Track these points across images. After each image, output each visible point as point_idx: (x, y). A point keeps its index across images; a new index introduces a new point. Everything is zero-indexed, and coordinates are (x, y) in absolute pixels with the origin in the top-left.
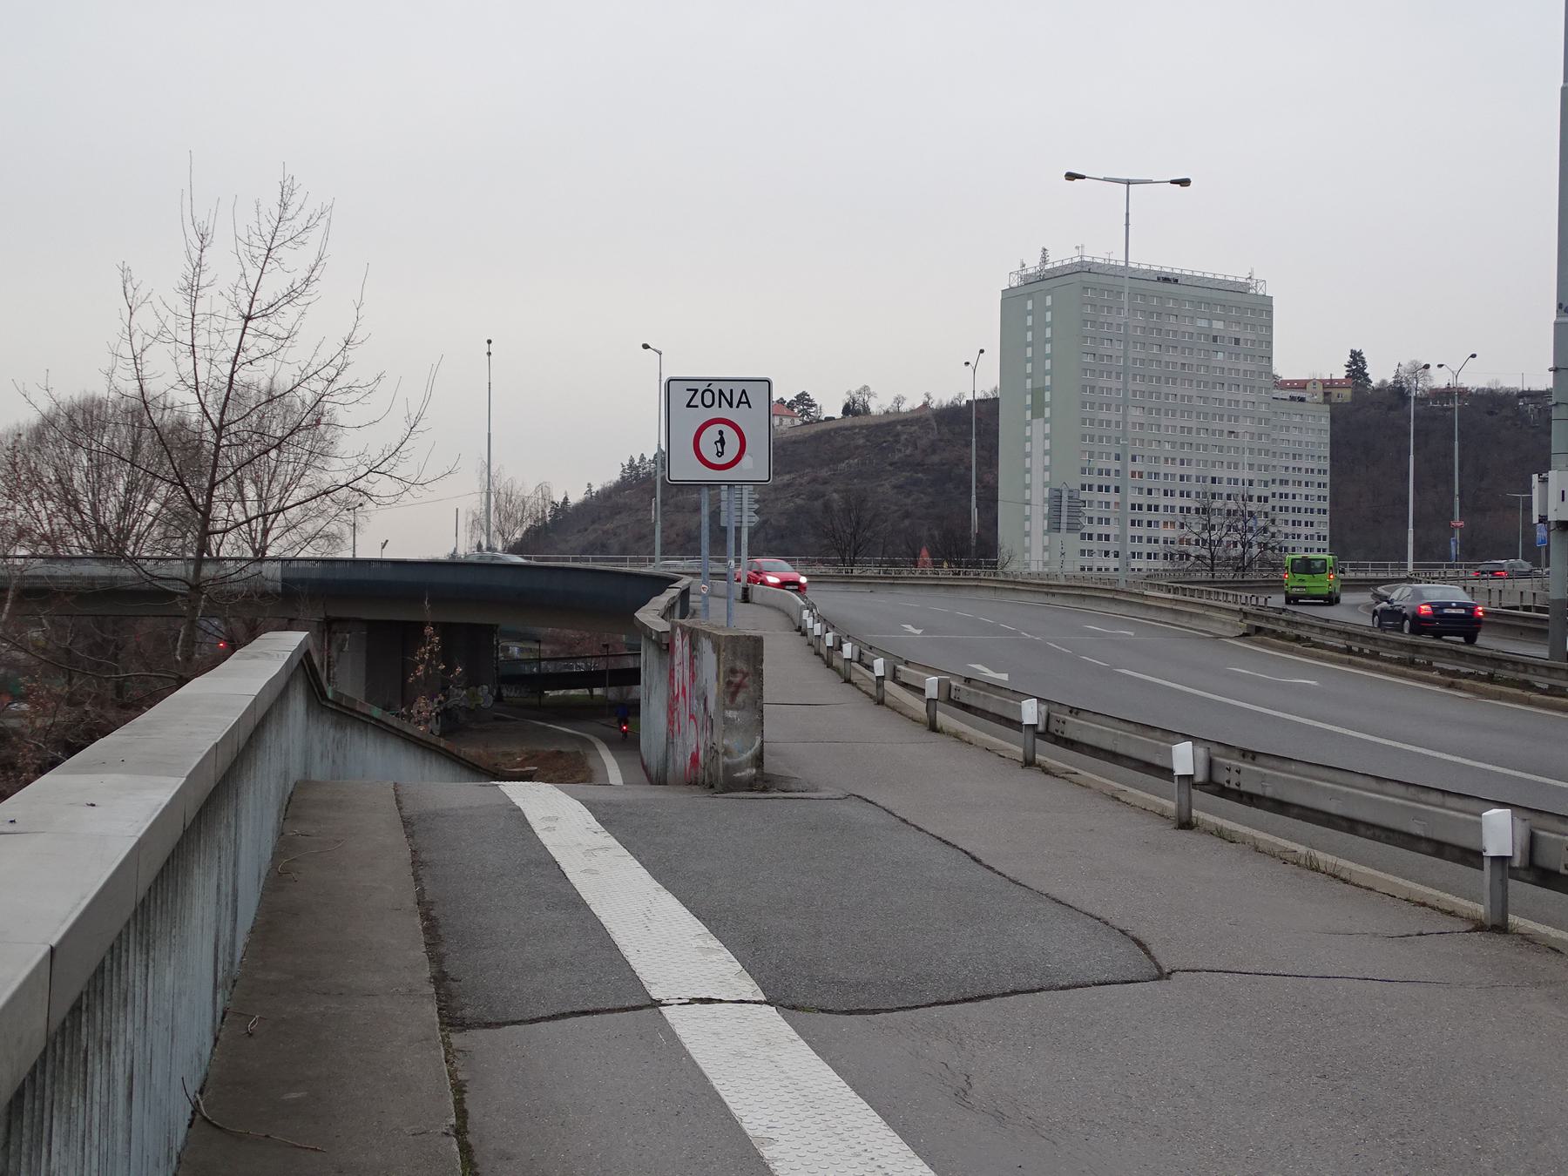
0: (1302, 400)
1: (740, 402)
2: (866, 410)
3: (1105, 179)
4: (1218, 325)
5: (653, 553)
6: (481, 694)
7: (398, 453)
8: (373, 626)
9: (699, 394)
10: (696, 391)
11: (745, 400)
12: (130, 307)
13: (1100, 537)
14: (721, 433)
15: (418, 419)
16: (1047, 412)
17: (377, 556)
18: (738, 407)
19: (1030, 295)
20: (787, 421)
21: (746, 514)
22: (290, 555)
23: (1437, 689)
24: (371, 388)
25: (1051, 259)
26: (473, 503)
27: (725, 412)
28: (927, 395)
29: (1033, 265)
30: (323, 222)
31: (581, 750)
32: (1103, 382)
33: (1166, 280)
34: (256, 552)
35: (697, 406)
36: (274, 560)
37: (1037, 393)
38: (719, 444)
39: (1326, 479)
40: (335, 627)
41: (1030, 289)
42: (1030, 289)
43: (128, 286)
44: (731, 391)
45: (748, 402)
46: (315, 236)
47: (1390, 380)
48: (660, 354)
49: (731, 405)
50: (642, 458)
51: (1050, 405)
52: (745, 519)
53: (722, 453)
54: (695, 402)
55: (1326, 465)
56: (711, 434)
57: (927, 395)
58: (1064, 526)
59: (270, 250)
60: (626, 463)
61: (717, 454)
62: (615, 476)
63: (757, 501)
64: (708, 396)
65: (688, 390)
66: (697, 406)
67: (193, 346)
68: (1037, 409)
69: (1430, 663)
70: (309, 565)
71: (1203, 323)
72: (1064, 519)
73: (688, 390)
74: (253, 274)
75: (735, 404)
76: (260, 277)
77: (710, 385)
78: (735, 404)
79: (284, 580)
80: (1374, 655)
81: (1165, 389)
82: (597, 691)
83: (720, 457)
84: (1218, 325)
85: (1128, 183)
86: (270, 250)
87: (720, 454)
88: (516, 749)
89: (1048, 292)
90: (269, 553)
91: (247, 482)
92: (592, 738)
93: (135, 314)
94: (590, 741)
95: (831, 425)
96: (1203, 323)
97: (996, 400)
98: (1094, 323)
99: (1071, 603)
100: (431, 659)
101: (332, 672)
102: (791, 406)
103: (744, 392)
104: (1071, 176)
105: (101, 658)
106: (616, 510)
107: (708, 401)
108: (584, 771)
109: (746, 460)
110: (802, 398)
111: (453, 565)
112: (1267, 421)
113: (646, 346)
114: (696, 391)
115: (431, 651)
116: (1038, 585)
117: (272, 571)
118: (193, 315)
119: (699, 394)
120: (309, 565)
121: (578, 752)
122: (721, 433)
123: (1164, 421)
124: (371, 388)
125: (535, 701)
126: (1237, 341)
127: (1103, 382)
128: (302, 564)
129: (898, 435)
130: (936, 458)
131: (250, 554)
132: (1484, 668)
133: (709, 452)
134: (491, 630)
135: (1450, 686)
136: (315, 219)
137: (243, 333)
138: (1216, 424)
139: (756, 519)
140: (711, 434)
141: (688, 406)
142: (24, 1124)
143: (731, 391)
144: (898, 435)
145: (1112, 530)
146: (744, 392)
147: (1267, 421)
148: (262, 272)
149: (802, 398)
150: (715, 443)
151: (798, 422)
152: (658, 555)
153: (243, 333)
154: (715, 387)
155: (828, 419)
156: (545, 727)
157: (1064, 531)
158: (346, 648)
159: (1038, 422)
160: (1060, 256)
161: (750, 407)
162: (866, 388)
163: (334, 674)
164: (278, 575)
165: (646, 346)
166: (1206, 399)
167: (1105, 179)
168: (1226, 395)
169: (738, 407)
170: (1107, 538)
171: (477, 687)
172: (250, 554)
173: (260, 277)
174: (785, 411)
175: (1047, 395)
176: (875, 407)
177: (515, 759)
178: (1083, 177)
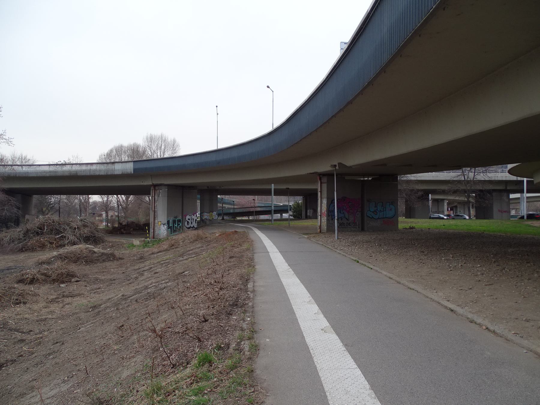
6: (214, 215)
8: (169, 186)
31: (246, 231)
40: (157, 188)
48: (273, 92)
88: (216, 231)
94: (250, 228)
101: (155, 204)
108: (249, 242)
113: (268, 87)
121: (245, 231)
142: (400, 210)
156: (234, 225)
158: (160, 196)
163: (156, 205)
165: (268, 87)
171: (212, 212)
177: (215, 235)
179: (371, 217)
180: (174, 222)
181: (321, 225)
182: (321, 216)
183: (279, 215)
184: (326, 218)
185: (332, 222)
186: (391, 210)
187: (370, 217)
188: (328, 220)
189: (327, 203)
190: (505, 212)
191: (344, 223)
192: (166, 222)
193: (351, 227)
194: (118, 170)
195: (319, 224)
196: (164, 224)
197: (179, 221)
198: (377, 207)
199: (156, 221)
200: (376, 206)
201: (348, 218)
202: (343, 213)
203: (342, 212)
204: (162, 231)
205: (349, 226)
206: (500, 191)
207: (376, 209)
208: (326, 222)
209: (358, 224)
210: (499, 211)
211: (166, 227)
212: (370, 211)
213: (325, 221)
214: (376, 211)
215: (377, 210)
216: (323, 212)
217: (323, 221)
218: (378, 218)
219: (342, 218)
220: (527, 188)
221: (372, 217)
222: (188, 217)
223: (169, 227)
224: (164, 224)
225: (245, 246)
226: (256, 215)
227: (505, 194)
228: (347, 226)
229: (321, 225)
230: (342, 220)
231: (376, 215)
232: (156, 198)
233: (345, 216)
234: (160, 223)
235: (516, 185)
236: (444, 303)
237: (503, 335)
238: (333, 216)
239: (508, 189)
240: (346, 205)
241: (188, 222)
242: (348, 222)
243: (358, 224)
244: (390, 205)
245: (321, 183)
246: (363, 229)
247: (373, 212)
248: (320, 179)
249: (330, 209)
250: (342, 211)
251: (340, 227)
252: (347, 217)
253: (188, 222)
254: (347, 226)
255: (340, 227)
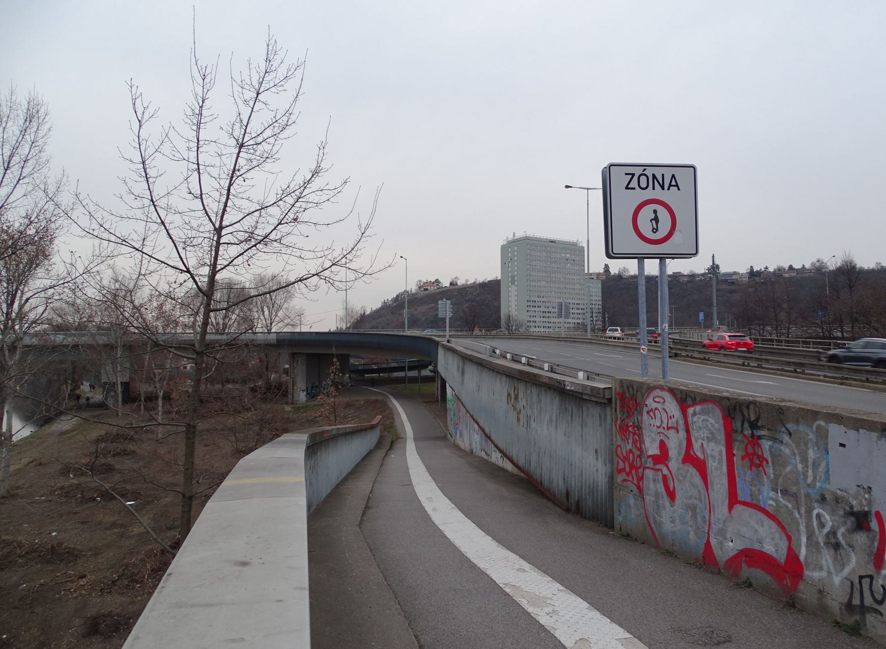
0: (592, 279)
1: (670, 185)
2: (457, 284)
3: (580, 188)
4: (568, 255)
5: (404, 328)
7: (354, 252)
8: (308, 355)
9: (636, 178)
10: (633, 175)
11: (674, 183)
12: (140, 121)
13: (533, 322)
14: (655, 212)
15: (368, 226)
16: (516, 283)
17: (308, 331)
18: (669, 189)
19: (510, 247)
20: (432, 288)
21: (448, 313)
22: (279, 331)
23: (836, 385)
24: (339, 189)
25: (516, 236)
26: (341, 313)
27: (657, 193)
28: (476, 279)
29: (511, 237)
30: (299, 73)
32: (533, 273)
33: (552, 242)
34: (268, 330)
35: (634, 189)
36: (274, 333)
37: (513, 277)
38: (654, 222)
39: (601, 303)
40: (295, 356)
41: (510, 245)
42: (510, 245)
43: (138, 102)
44: (663, 175)
45: (677, 185)
46: (291, 86)
47: (617, 273)
49: (663, 187)
50: (388, 300)
51: (516, 281)
52: (447, 315)
53: (657, 230)
54: (634, 184)
55: (600, 299)
56: (646, 213)
57: (476, 279)
58: (563, 316)
59: (258, 94)
60: (383, 301)
61: (653, 231)
62: (380, 306)
63: (452, 308)
64: (643, 180)
65: (626, 174)
66: (634, 189)
67: (198, 164)
68: (513, 283)
69: (803, 371)
70: (286, 334)
71: (564, 255)
72: (563, 313)
73: (626, 174)
74: (245, 112)
75: (666, 186)
76: (251, 115)
77: (644, 170)
78: (666, 186)
79: (277, 340)
80: (760, 366)
81: (552, 275)
82: (382, 375)
83: (655, 233)
84: (568, 255)
85: (588, 189)
86: (258, 94)
87: (655, 230)
89: (515, 246)
90: (272, 331)
91: (265, 307)
92: (387, 394)
93: (143, 127)
95: (446, 288)
96: (564, 255)
97: (500, 280)
98: (530, 255)
99: (556, 342)
100: (336, 372)
102: (433, 283)
103: (673, 176)
104: (567, 187)
105: (207, 374)
106: (380, 317)
107: (643, 184)
109: (676, 235)
110: (437, 281)
111: (338, 334)
112: (584, 285)
113: (401, 257)
114: (633, 175)
115: (336, 368)
116: (553, 337)
117: (273, 337)
118: (198, 141)
119: (636, 178)
120: (286, 334)
122: (655, 212)
123: (552, 286)
124: (339, 189)
125: (362, 378)
126: (574, 260)
127: (533, 273)
128: (283, 334)
129: (467, 291)
130: (478, 299)
131: (266, 331)
132: (864, 375)
133: (646, 228)
134: (348, 356)
135: (842, 384)
136: (293, 70)
137: (238, 156)
138: (568, 286)
139: (451, 315)
140: (646, 213)
141: (627, 188)
143: (663, 175)
144: (467, 291)
145: (537, 319)
146: (673, 176)
147: (584, 285)
148: (252, 111)
149: (437, 281)
150: (651, 221)
151: (436, 288)
152: (406, 329)
153: (238, 156)
154: (649, 172)
155: (445, 287)
157: (563, 317)
158: (299, 363)
159: (513, 286)
160: (520, 234)
161: (679, 189)
162: (457, 277)
164: (275, 338)
165: (401, 257)
166: (565, 279)
167: (580, 188)
168: (571, 277)
169: (669, 189)
170: (535, 322)
172: (266, 331)
173: (251, 115)
174: (432, 285)
175: (516, 278)
176: (460, 283)
178: (571, 187)
180: (312, 388)
192: (305, 388)
194: (261, 340)
196: (303, 391)
197: (317, 387)
199: (295, 388)
204: (302, 397)
211: (305, 393)
222: (324, 383)
223: (308, 394)
224: (303, 391)
225: (388, 412)
226: (389, 372)
232: (295, 365)
234: (299, 389)
236: (661, 488)
241: (324, 388)
253: (324, 388)
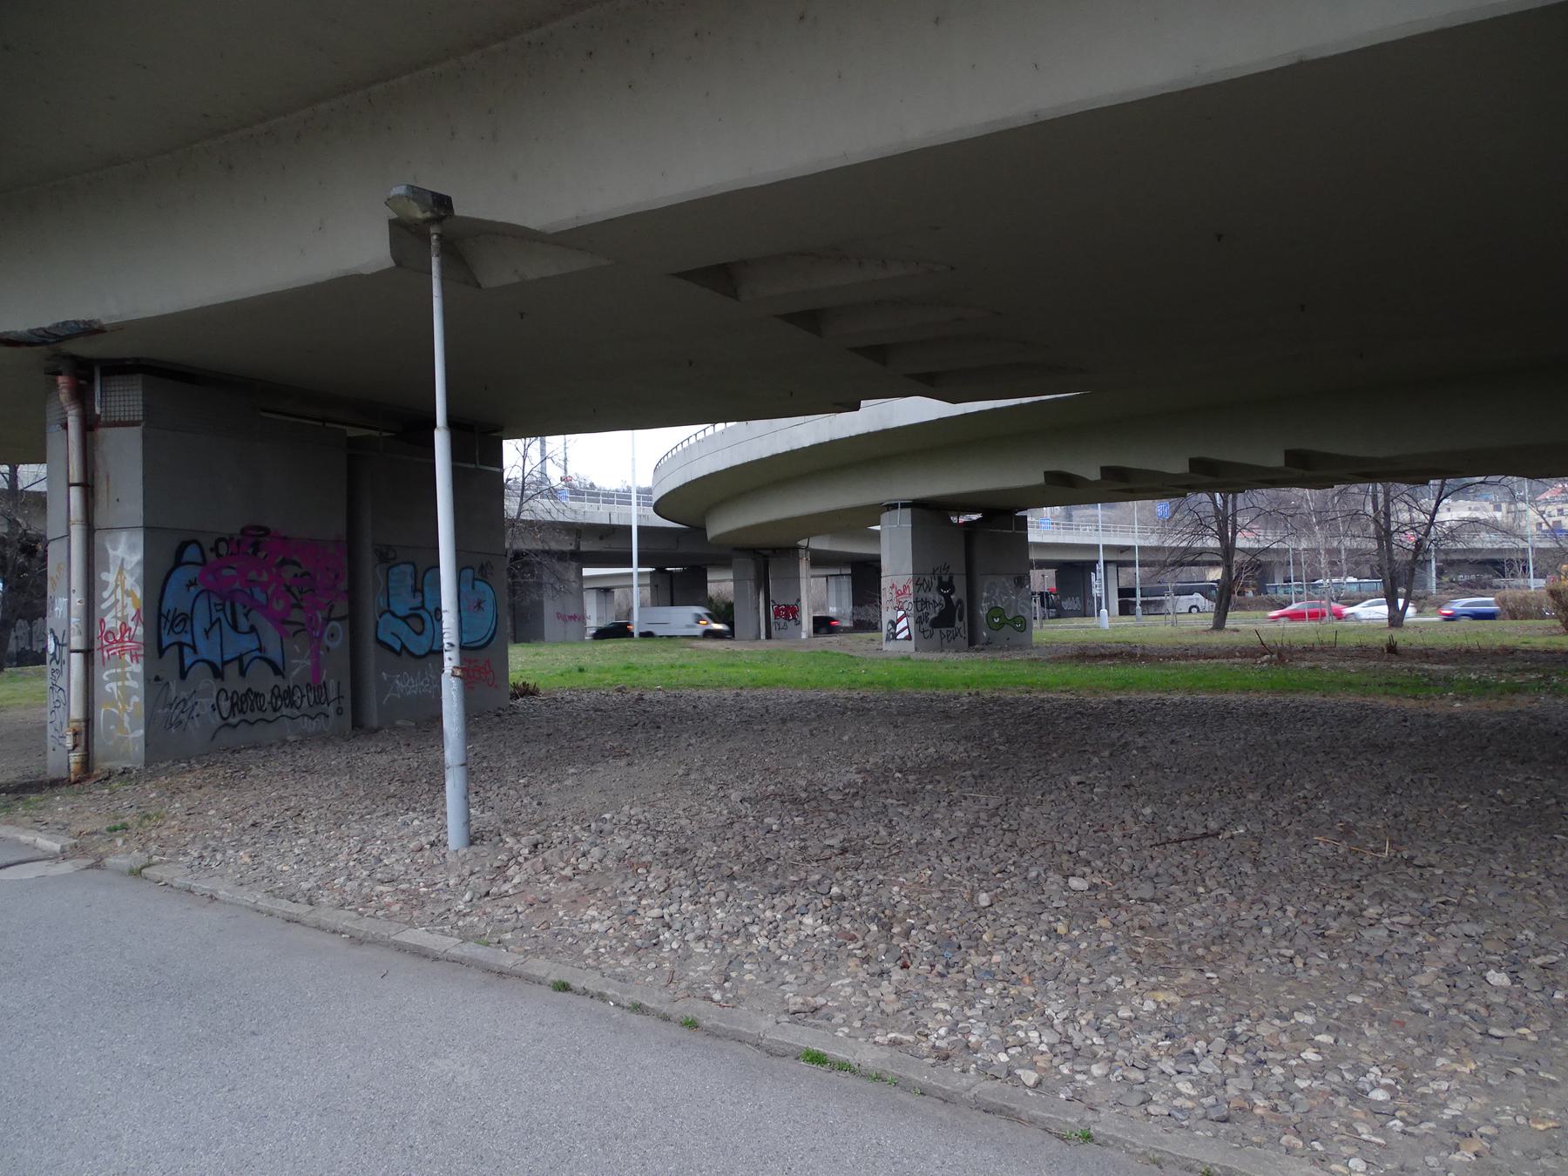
179: (397, 647)
181: (89, 720)
182: (88, 653)
183: (583, 548)
184: (137, 668)
185: (184, 694)
186: (479, 604)
187: (391, 649)
188: (153, 681)
189: (147, 563)
190: (573, 617)
191: (257, 695)
193: (297, 713)
195: (76, 712)
198: (422, 592)
200: (419, 586)
201: (279, 662)
202: (253, 629)
203: (244, 624)
205: (285, 711)
206: (562, 556)
207: (417, 602)
208: (138, 699)
209: (333, 695)
210: (559, 616)
212: (393, 614)
213: (127, 693)
214: (419, 612)
215: (423, 607)
216: (111, 622)
217: (112, 687)
218: (427, 650)
219: (246, 660)
220: (638, 549)
221: (403, 646)
227: (574, 565)
228: (275, 710)
229: (89, 720)
230: (243, 673)
231: (419, 634)
233: (260, 649)
235: (601, 538)
237: (671, 1015)
238: (187, 650)
239: (584, 552)
240: (265, 577)
242: (283, 687)
243: (333, 695)
244: (477, 583)
245: (89, 426)
246: (359, 726)
247: (404, 619)
248: (82, 396)
249: (168, 604)
250: (246, 615)
251: (233, 721)
252: (273, 652)
254: (275, 710)
255: (233, 721)
